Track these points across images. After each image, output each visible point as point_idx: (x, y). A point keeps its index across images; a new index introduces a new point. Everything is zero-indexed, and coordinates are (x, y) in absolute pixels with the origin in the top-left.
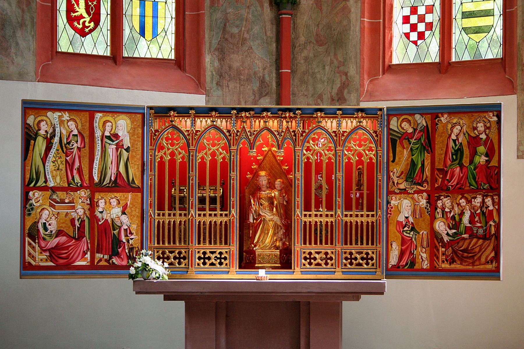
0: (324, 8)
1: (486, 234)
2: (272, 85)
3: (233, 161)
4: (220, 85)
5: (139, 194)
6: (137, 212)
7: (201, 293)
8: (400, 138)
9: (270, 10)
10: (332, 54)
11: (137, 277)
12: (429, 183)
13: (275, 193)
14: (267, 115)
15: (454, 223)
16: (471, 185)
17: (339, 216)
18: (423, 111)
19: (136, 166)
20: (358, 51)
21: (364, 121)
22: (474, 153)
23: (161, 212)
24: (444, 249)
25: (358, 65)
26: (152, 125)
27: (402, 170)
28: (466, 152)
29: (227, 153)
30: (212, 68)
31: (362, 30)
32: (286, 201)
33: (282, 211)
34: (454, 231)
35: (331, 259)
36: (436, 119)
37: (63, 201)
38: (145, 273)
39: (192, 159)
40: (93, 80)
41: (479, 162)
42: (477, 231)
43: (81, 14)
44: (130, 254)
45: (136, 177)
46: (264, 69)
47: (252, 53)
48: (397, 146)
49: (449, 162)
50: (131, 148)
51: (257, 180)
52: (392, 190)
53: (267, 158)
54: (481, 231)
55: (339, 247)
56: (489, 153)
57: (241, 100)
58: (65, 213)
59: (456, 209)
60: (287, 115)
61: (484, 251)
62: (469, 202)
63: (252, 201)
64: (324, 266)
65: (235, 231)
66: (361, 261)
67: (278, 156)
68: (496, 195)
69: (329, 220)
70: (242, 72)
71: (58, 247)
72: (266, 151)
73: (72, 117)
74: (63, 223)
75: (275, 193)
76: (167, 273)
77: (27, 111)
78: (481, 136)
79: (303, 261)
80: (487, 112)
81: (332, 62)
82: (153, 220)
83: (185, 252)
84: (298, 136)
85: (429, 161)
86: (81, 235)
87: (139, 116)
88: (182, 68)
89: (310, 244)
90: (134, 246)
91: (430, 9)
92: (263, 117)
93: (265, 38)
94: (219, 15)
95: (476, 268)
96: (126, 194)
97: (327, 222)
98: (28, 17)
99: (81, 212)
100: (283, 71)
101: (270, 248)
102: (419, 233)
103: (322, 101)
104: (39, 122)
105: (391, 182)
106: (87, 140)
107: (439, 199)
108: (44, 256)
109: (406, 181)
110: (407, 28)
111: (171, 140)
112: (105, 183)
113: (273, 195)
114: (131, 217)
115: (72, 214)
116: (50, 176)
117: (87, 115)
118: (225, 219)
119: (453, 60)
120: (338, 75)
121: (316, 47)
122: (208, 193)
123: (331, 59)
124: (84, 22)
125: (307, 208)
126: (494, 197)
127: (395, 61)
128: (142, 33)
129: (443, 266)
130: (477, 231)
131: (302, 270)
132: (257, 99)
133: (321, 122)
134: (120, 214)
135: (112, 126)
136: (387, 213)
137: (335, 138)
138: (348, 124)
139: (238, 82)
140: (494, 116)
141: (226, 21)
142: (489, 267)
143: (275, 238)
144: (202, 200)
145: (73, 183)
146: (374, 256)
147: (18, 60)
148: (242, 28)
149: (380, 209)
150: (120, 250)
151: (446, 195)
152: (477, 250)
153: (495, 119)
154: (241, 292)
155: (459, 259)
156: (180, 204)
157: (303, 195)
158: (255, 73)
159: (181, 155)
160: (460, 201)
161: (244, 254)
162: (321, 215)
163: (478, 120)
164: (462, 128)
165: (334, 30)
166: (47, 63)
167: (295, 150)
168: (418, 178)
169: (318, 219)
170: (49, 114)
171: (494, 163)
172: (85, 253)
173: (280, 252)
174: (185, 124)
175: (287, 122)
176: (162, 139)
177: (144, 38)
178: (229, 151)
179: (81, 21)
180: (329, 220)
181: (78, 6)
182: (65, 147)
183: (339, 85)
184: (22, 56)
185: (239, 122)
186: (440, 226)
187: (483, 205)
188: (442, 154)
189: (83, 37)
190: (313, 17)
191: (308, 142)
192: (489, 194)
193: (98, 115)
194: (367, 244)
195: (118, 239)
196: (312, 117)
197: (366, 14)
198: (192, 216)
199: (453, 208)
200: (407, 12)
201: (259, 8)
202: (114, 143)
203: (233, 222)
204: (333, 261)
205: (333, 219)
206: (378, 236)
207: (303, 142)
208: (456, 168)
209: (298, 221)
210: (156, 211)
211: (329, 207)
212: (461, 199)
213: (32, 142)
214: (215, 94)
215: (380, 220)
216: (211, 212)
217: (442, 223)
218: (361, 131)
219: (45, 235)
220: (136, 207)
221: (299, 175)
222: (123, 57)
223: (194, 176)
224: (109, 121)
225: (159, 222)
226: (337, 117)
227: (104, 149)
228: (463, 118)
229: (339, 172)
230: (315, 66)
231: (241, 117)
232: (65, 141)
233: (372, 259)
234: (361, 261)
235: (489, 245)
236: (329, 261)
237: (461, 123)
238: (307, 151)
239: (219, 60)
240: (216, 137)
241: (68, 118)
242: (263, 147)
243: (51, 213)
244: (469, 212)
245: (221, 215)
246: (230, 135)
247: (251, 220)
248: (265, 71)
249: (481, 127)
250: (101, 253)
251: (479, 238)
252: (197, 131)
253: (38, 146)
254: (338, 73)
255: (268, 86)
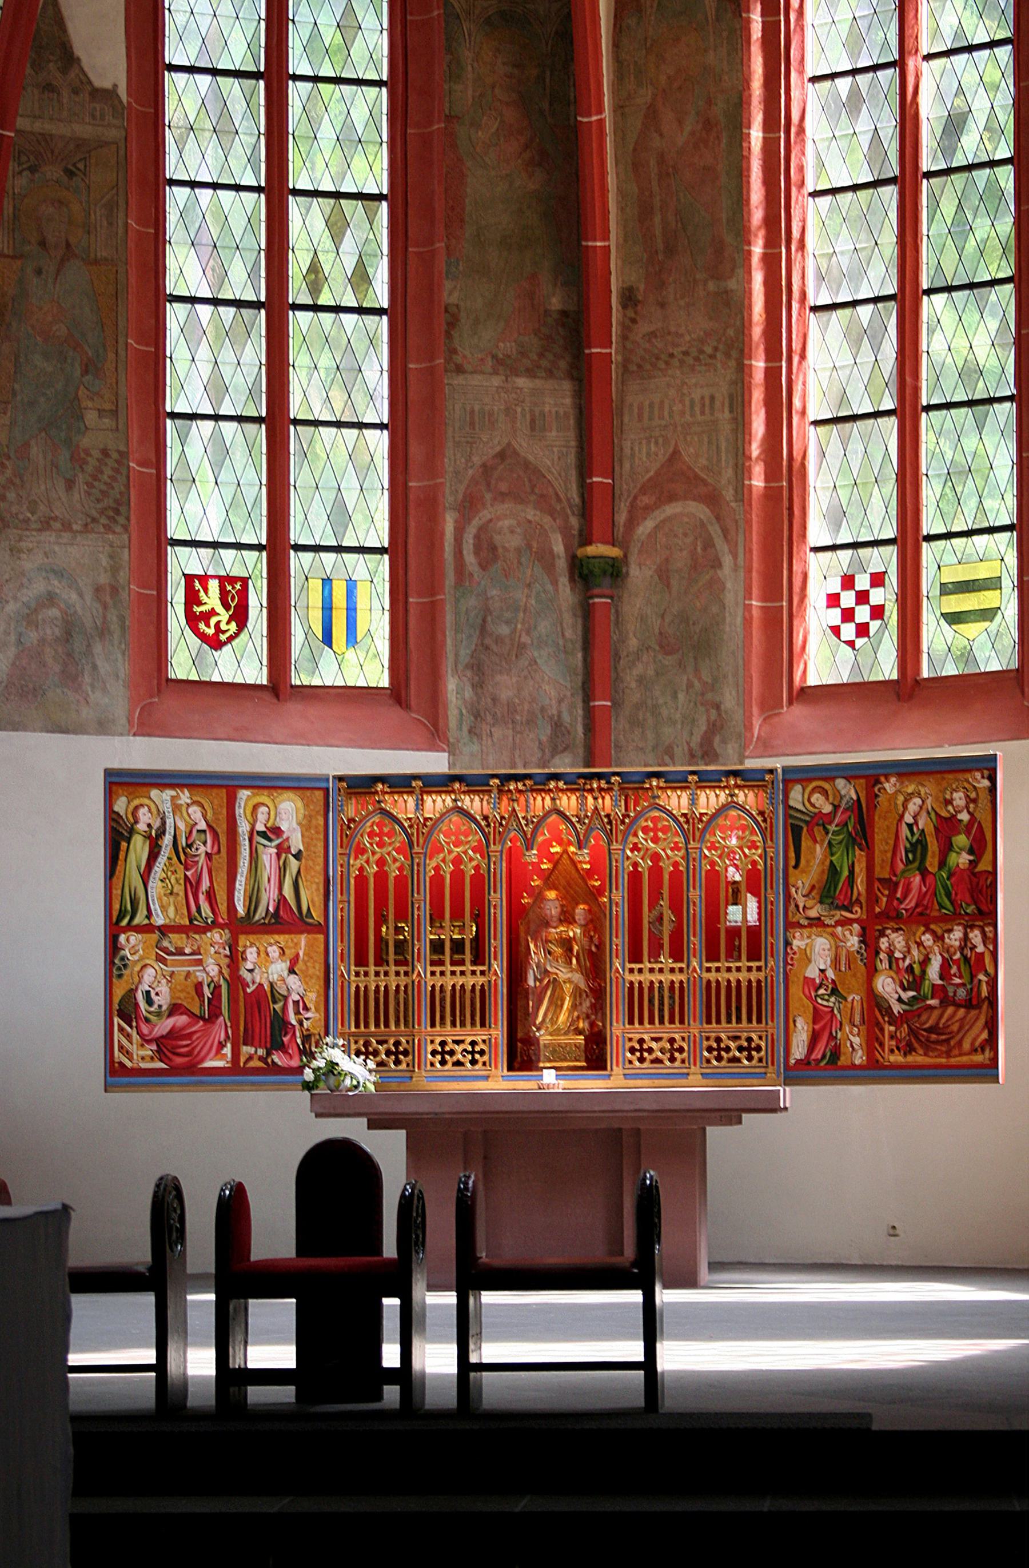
0: (674, 582)
1: (970, 999)
2: (576, 730)
3: (495, 872)
4: (475, 734)
5: (321, 937)
6: (318, 970)
7: (436, 1114)
8: (807, 823)
9: (571, 589)
10: (690, 669)
11: (317, 1087)
12: (864, 905)
13: (575, 931)
14: (557, 787)
15: (911, 979)
16: (941, 906)
17: (694, 970)
18: (851, 773)
19: (314, 886)
20: (741, 663)
21: (741, 795)
22: (947, 848)
23: (362, 970)
24: (892, 1028)
25: (741, 689)
26: (343, 810)
27: (814, 882)
28: (933, 846)
29: (482, 856)
30: (460, 702)
31: (748, 621)
32: (596, 946)
33: (588, 964)
34: (912, 993)
35: (681, 1050)
36: (874, 786)
37: (180, 952)
38: (332, 1080)
39: (418, 871)
40: (236, 729)
41: (958, 865)
42: (955, 992)
43: (213, 609)
44: (304, 1047)
45: (314, 906)
46: (560, 701)
47: (535, 671)
48: (803, 838)
49: (901, 866)
50: (304, 854)
51: (540, 908)
52: (794, 920)
53: (560, 867)
54: (962, 993)
55: (694, 1029)
56: (975, 846)
57: (517, 760)
58: (184, 974)
59: (915, 952)
60: (595, 786)
61: (971, 1027)
62: (939, 938)
63: (532, 946)
64: (668, 1063)
65: (500, 1002)
66: (737, 1054)
67: (580, 862)
68: (989, 924)
69: (677, 977)
70: (518, 708)
71: (174, 1034)
72: (557, 853)
73: (195, 798)
74: (181, 991)
75: (575, 931)
76: (373, 1078)
77: (114, 788)
78: (960, 817)
79: (628, 1055)
80: (969, 771)
81: (690, 685)
82: (346, 984)
83: (408, 1042)
84: (616, 824)
85: (864, 864)
86: (215, 1013)
87: (319, 794)
88: (404, 705)
89: (641, 1023)
90: (312, 1031)
91: (877, 580)
92: (550, 790)
93: (561, 642)
94: (472, 602)
95: (953, 1061)
96: (295, 937)
97: (672, 982)
98: (115, 618)
99: (213, 970)
100: (597, 703)
101: (566, 1034)
102: (845, 999)
103: (672, 758)
104: (137, 808)
105: (793, 905)
106: (223, 839)
107: (882, 934)
108: (148, 1051)
109: (821, 902)
110: (834, 616)
111: (379, 837)
112: (257, 918)
113: (571, 934)
114: (305, 978)
115: (198, 974)
116: (157, 906)
117: (223, 792)
118: (481, 980)
119: (925, 674)
120: (702, 709)
121: (660, 657)
122: (449, 934)
123: (688, 679)
124: (218, 623)
125: (635, 956)
126: (987, 929)
127: (812, 681)
128: (328, 639)
129: (892, 1058)
130: (955, 992)
131: (627, 1072)
132: (547, 757)
133: (659, 797)
134: (286, 973)
135: (269, 814)
136: (786, 963)
137: (686, 827)
138: (709, 800)
139: (510, 726)
140: (983, 777)
141: (487, 611)
142: (978, 1058)
143: (576, 1014)
144: (437, 947)
145: (199, 918)
146: (763, 1044)
147: (96, 696)
148: (516, 626)
149: (772, 956)
150: (286, 1039)
151: (896, 926)
152: (955, 1028)
153: (986, 783)
154: (511, 1112)
155: (921, 1046)
156: (396, 954)
157: (626, 933)
158: (543, 709)
159: (398, 864)
160: (923, 938)
161: (519, 1044)
162: (661, 970)
163: (954, 786)
164: (923, 801)
165: (694, 624)
166: (149, 701)
167: (609, 850)
168: (842, 897)
169: (655, 977)
170: (154, 793)
171: (984, 866)
172: (221, 1046)
173: (585, 1040)
174: (404, 807)
175: (595, 799)
176: (362, 836)
177: (331, 647)
178: (486, 854)
179: (213, 621)
180: (677, 977)
181: (206, 592)
182: (183, 853)
183: (704, 728)
184: (104, 690)
185: (505, 801)
186: (886, 985)
187: (966, 945)
188: (886, 852)
189: (216, 650)
190: (653, 601)
191: (636, 835)
192: (977, 923)
193: (244, 794)
194: (750, 1021)
195: (283, 1020)
196: (643, 788)
197: (755, 591)
198: (419, 974)
199: (909, 952)
200: (834, 586)
201: (549, 587)
202: (274, 844)
203: (496, 984)
204: (685, 1054)
205: (683, 977)
206: (769, 1007)
207: (625, 834)
208: (914, 876)
209: (617, 982)
210: (353, 968)
211: (677, 954)
212: (924, 933)
213: (124, 844)
214: (466, 750)
215: (772, 976)
216: (454, 968)
217: (890, 980)
218: (733, 813)
219: (149, 1013)
220: (316, 961)
221: (620, 896)
222: (292, 686)
223: (422, 904)
224: (263, 804)
225: (358, 988)
226: (688, 788)
227: (254, 855)
228: (926, 783)
229: (694, 888)
230: (657, 693)
231: (509, 791)
232: (183, 842)
233: (758, 1049)
234: (737, 1054)
235: (977, 1019)
236: (677, 1054)
237: (922, 793)
238: (632, 850)
239: (473, 686)
240: (463, 828)
241: (189, 801)
242: (552, 846)
243: (159, 972)
244: (939, 958)
245: (474, 973)
246: (488, 825)
247: (531, 982)
248: (563, 705)
249: (959, 798)
250: (252, 1045)
251: (958, 1005)
252: (426, 819)
253: (135, 851)
254: (702, 704)
255: (569, 732)
